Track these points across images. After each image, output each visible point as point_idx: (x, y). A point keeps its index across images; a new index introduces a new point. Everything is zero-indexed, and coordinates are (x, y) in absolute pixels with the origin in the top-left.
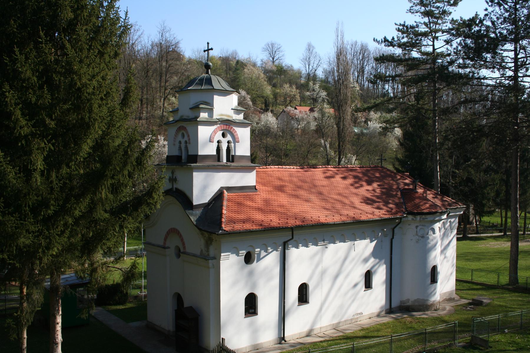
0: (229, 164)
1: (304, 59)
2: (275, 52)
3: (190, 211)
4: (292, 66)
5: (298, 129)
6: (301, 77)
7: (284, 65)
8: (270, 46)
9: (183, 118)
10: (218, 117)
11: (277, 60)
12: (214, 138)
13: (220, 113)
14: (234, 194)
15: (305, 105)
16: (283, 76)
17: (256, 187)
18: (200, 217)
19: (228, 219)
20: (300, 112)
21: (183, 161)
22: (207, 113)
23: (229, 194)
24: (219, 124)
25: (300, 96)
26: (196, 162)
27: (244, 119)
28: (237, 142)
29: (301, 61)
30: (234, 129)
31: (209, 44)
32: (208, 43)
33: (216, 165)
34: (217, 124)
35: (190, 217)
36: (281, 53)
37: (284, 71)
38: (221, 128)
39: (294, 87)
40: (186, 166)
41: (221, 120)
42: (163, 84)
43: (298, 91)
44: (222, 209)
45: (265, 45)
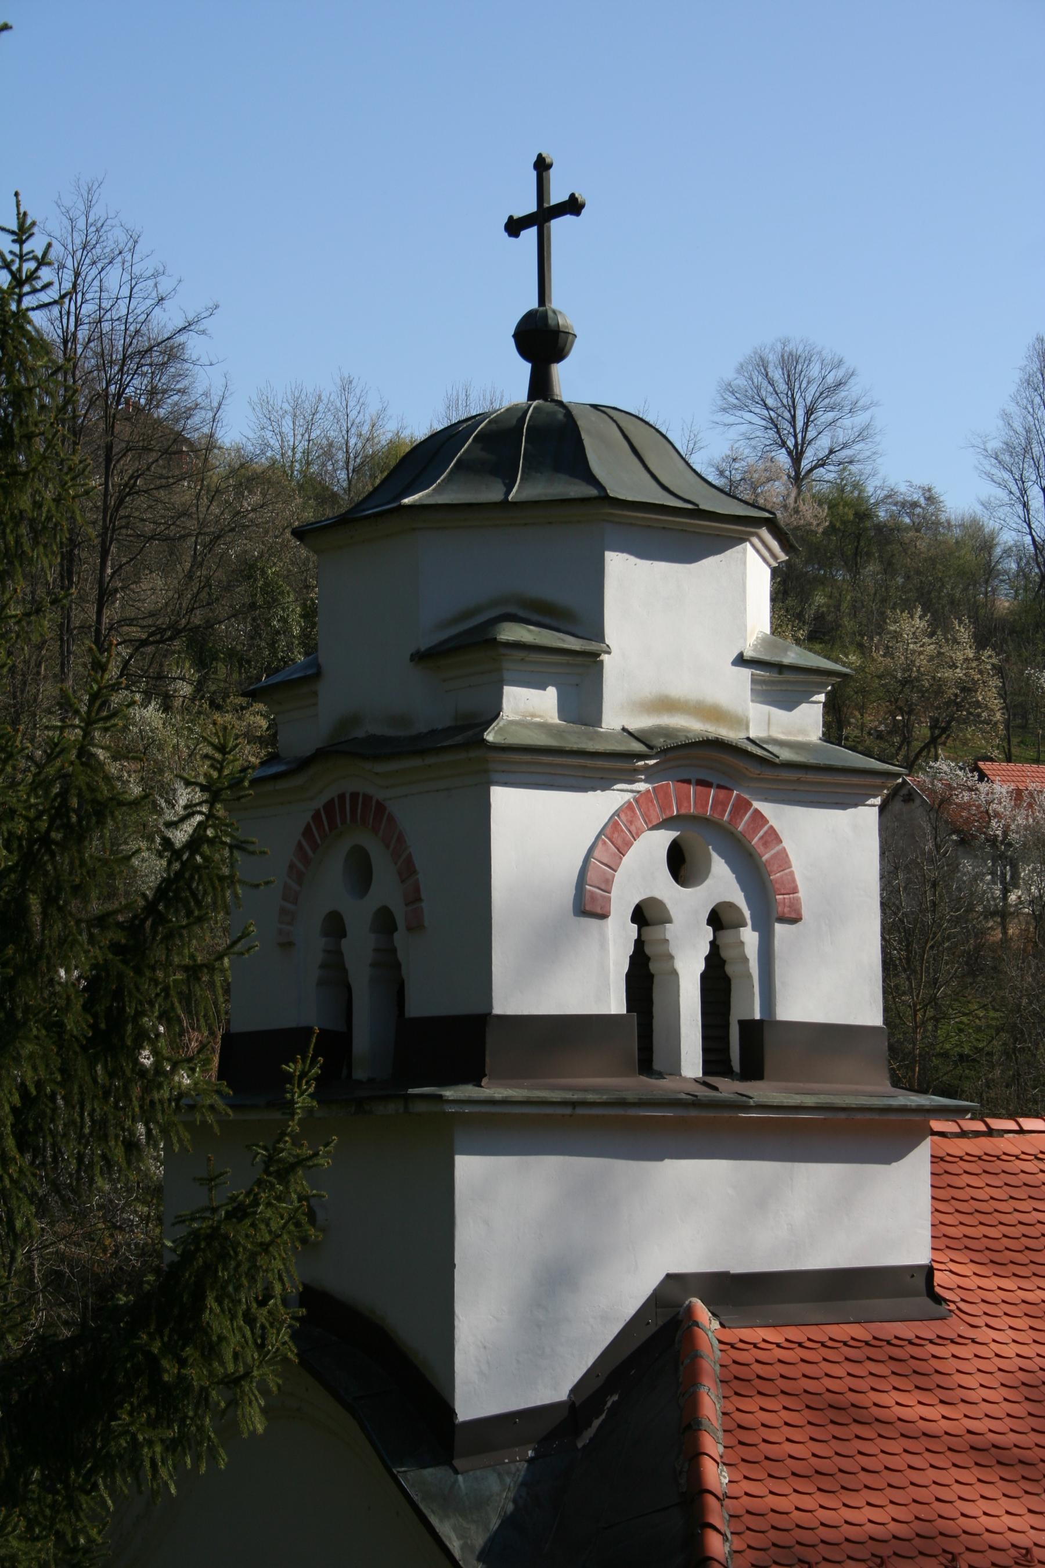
0: (728, 1088)
1: (1009, 448)
2: (810, 412)
3: (428, 1472)
4: (931, 499)
5: (1003, 914)
6: (990, 572)
7: (873, 489)
8: (777, 375)
9: (360, 733)
10: (639, 723)
11: (822, 463)
12: (606, 886)
13: (648, 687)
14: (773, 1335)
15: (1032, 754)
16: (871, 569)
17: (939, 1277)
18: (509, 1522)
19: (751, 1538)
20: (1018, 795)
21: (359, 1074)
22: (552, 692)
23: (732, 1335)
24: (650, 775)
25: (1003, 694)
26: (476, 1080)
27: (827, 737)
28: (782, 920)
29: (989, 465)
30: (759, 818)
31: (553, 172)
32: (542, 166)
33: (630, 1097)
34: (630, 777)
35: (434, 1520)
36: (847, 422)
37: (880, 528)
38: (665, 806)
39: (964, 633)
40: (391, 1108)
41: (660, 742)
42: (84, 614)
43: (990, 657)
44: (696, 1454)
45: (741, 369)
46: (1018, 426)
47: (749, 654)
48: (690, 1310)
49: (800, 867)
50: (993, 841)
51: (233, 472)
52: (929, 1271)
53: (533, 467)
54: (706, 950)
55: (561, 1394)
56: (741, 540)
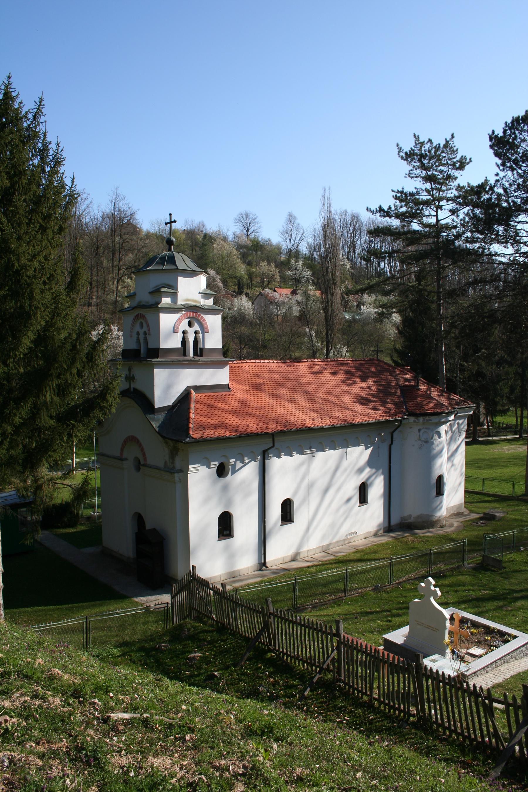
0: (197, 358)
1: (284, 231)
2: (250, 223)
4: (270, 240)
5: (278, 315)
6: (281, 253)
7: (260, 239)
8: (244, 217)
11: (252, 233)
12: (178, 328)
14: (203, 395)
17: (230, 385)
18: (162, 422)
20: (280, 295)
21: (142, 356)
23: (197, 395)
24: (185, 311)
25: (280, 276)
29: (280, 235)
30: (202, 317)
32: (170, 215)
33: (181, 360)
34: (182, 311)
37: (261, 246)
38: (187, 315)
39: (273, 265)
40: (145, 362)
41: (186, 306)
42: (116, 263)
43: (277, 270)
44: (189, 413)
46: (285, 227)
47: (201, 292)
48: (191, 391)
49: (208, 325)
50: (276, 303)
51: (146, 235)
52: (228, 385)
53: (167, 263)
54: (194, 337)
55: (171, 404)
56: (200, 274)
